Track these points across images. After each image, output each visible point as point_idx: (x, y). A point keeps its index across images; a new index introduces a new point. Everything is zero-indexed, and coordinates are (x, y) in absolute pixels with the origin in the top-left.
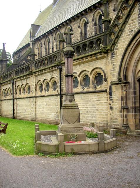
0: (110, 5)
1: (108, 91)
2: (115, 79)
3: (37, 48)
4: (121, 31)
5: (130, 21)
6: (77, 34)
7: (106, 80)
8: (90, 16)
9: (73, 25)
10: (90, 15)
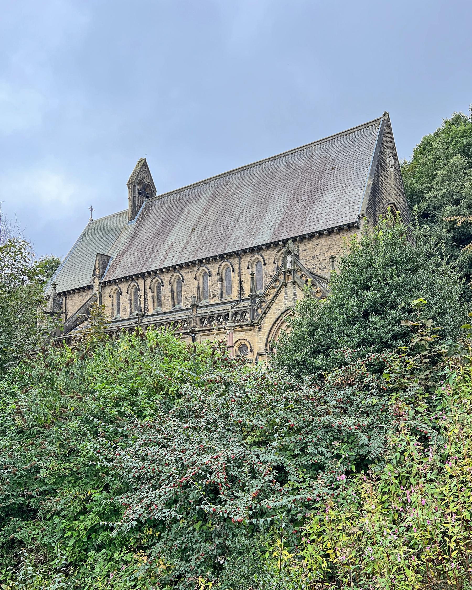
0: (242, 260)
1: (254, 361)
2: (262, 350)
3: (110, 296)
4: (269, 307)
5: (277, 301)
6: (191, 288)
7: (251, 351)
8: (213, 266)
9: (186, 273)
10: (213, 265)
